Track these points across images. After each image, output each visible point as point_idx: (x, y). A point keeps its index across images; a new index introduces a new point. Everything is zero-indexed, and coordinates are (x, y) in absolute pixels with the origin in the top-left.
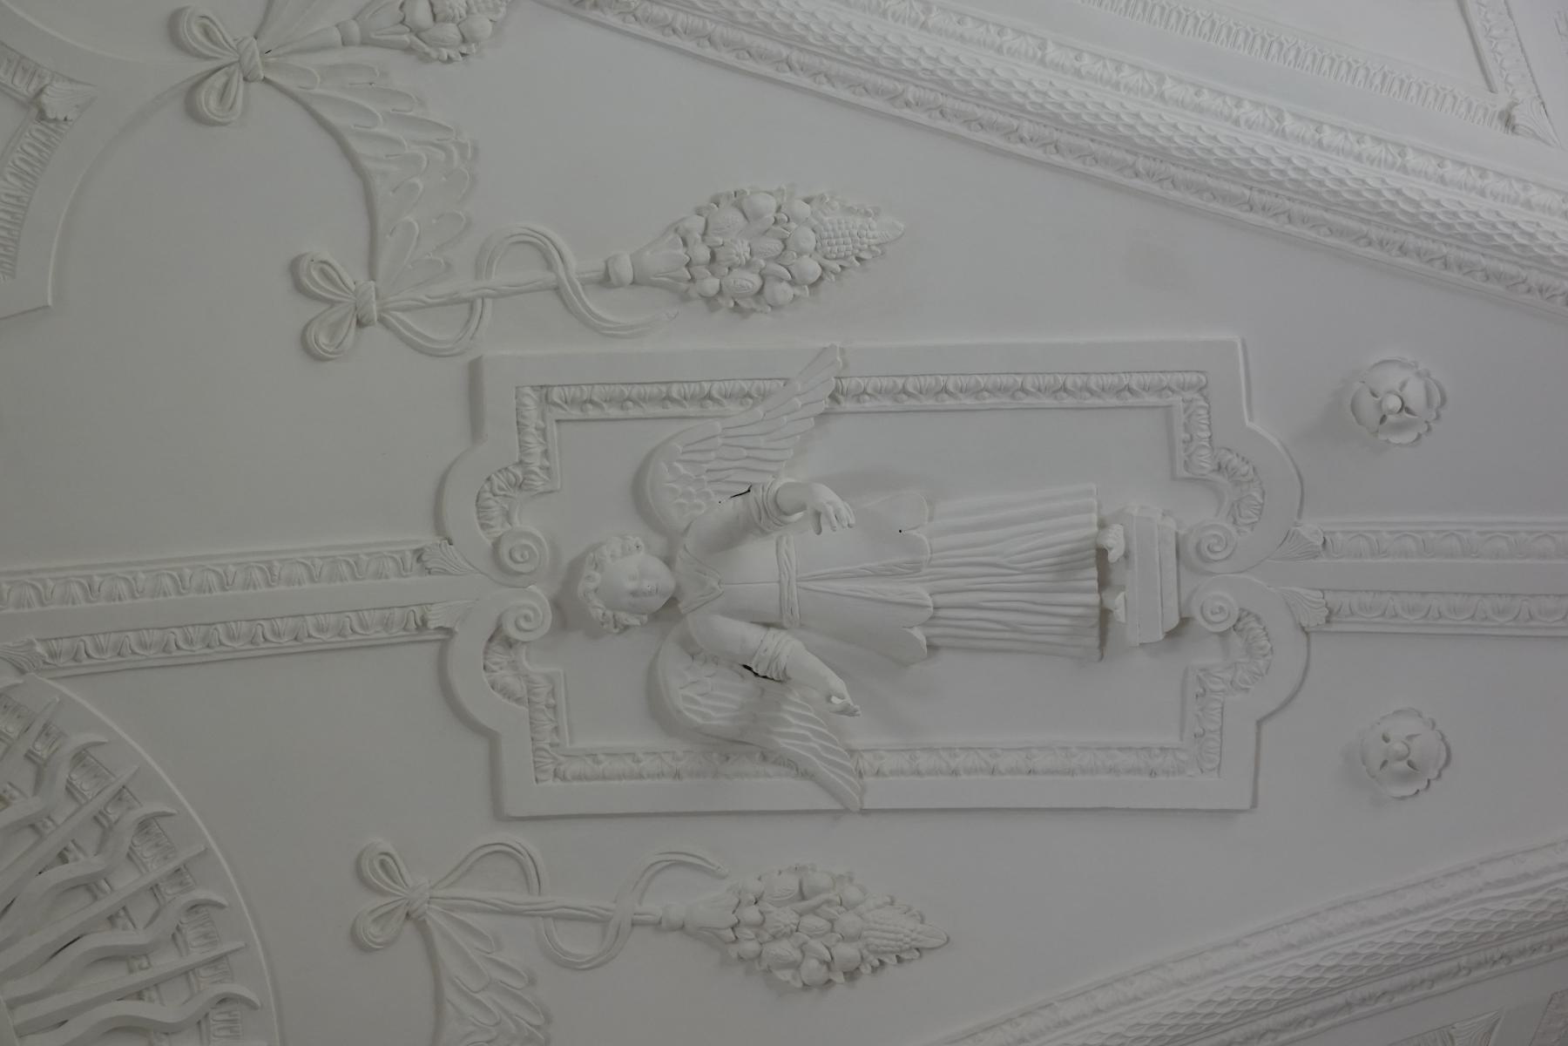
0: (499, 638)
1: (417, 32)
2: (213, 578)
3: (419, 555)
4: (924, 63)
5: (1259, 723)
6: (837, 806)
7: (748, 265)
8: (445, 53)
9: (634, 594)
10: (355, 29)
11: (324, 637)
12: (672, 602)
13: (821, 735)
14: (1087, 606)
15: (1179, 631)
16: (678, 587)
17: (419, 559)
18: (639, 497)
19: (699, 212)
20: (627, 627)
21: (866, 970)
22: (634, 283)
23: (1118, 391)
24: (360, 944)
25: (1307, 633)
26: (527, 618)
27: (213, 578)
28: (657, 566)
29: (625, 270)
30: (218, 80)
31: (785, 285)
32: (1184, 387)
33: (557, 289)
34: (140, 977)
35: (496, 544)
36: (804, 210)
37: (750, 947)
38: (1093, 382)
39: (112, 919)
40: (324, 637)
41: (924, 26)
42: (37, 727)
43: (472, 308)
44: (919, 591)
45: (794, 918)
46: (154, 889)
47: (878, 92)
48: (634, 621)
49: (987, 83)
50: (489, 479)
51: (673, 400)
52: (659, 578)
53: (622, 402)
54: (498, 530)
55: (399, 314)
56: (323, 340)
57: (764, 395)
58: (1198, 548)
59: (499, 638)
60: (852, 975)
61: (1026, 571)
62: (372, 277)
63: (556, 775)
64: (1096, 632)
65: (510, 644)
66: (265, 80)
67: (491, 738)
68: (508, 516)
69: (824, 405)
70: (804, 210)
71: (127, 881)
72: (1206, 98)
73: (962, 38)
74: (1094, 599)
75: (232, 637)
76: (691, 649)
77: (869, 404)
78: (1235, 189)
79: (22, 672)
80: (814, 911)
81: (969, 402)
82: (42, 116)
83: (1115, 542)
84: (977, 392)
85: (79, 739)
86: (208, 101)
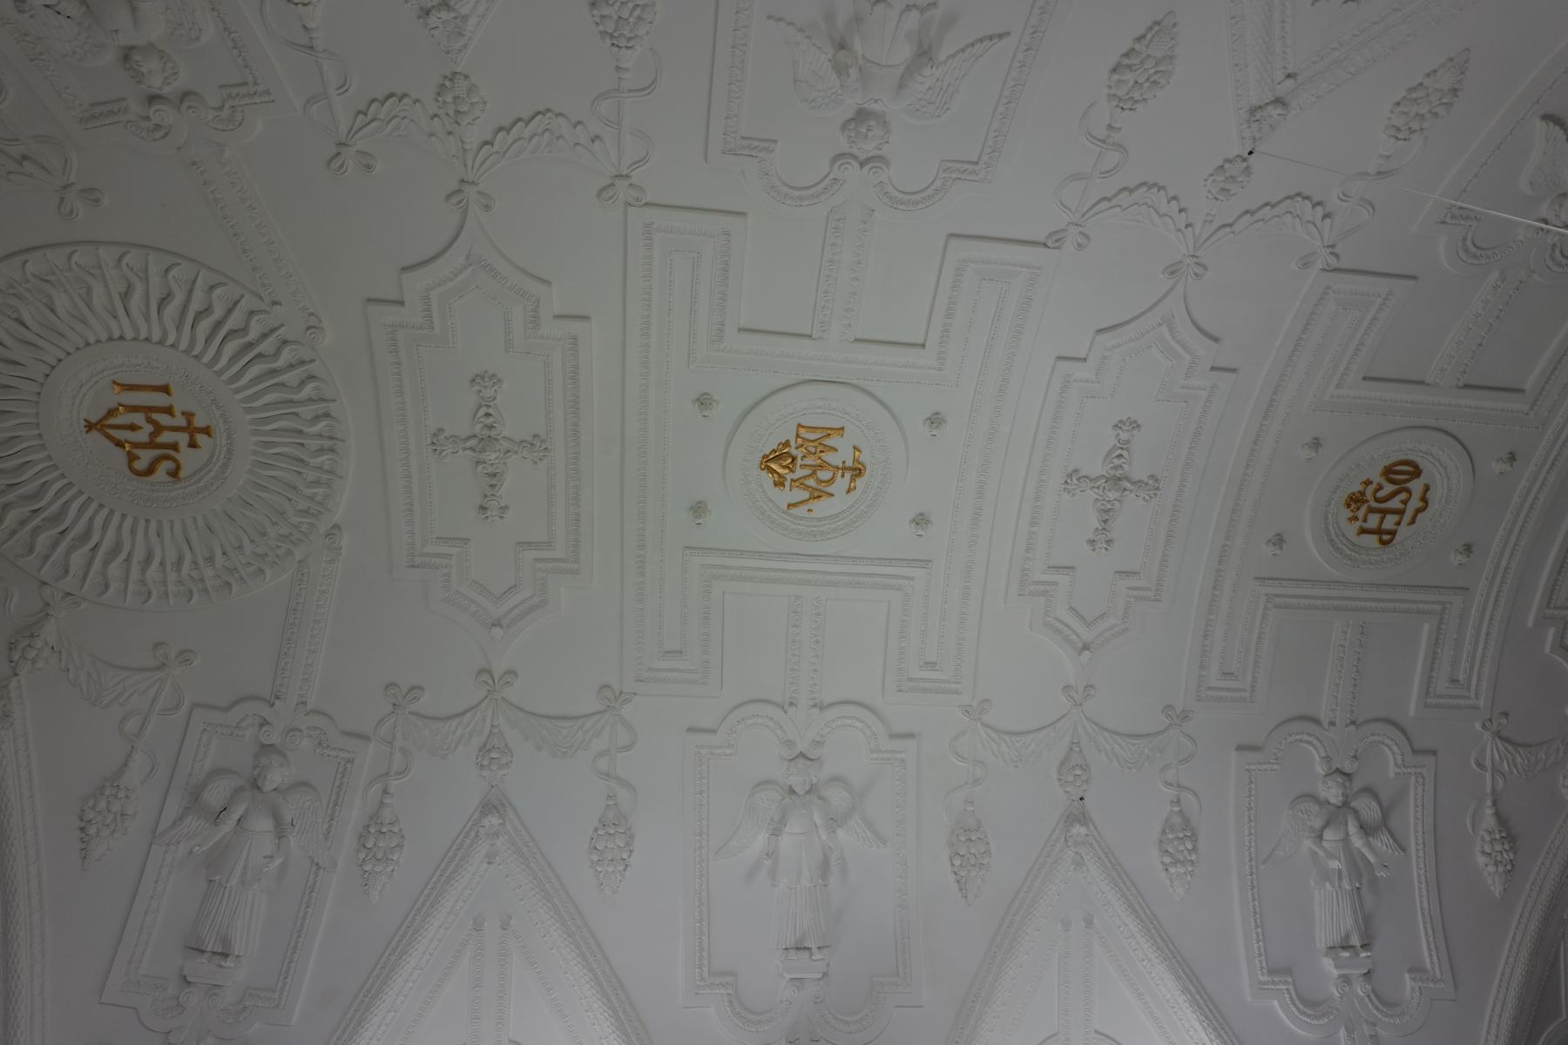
0: (264, 723)
1: (489, 751)
2: (322, 603)
3: (304, 703)
4: (427, 926)
5: (135, 1008)
6: (158, 832)
7: (375, 845)
8: (480, 758)
9: (265, 777)
10: (495, 731)
11: (283, 663)
12: (259, 788)
13: (189, 832)
14: (207, 947)
15: (185, 981)
16: (263, 792)
17: (302, 703)
18: (303, 784)
19: (400, 830)
20: (254, 768)
21: (83, 835)
22: (382, 802)
23: (287, 972)
24: (157, 645)
25: (167, 1033)
26: (268, 735)
27: (322, 603)
28: (274, 786)
29: (387, 801)
30: (490, 682)
31: (364, 856)
32: (280, 999)
33: (387, 774)
34: (168, 566)
35: (300, 731)
36: (389, 869)
37: (108, 792)
38: (293, 964)
39: (195, 562)
40: (283, 663)
41: (440, 927)
42: (276, 560)
43: (389, 743)
44: (234, 882)
45: (114, 810)
46: (202, 580)
47: (423, 905)
48: (256, 773)
49: (413, 947)
50: (325, 734)
51: (335, 806)
52: (268, 786)
53: (340, 787)
54: (305, 732)
55: (393, 720)
56: (392, 691)
57: (326, 839)
58: (215, 994)
59: (264, 723)
60: (82, 829)
61: (228, 926)
62: (410, 713)
63: (205, 730)
64: (196, 947)
65: (261, 725)
66: (487, 697)
67: (227, 709)
68: (309, 737)
69: (316, 860)
70: (389, 869)
71: (209, 573)
72: (384, 1027)
73: (432, 940)
74: (209, 949)
75: (298, 603)
76: (238, 790)
77: (312, 877)
78: (346, 1035)
79: (300, 562)
80: (115, 819)
81: (301, 914)
82: (494, 625)
83: (229, 963)
84: (304, 918)
85: (268, 573)
86: (485, 677)
